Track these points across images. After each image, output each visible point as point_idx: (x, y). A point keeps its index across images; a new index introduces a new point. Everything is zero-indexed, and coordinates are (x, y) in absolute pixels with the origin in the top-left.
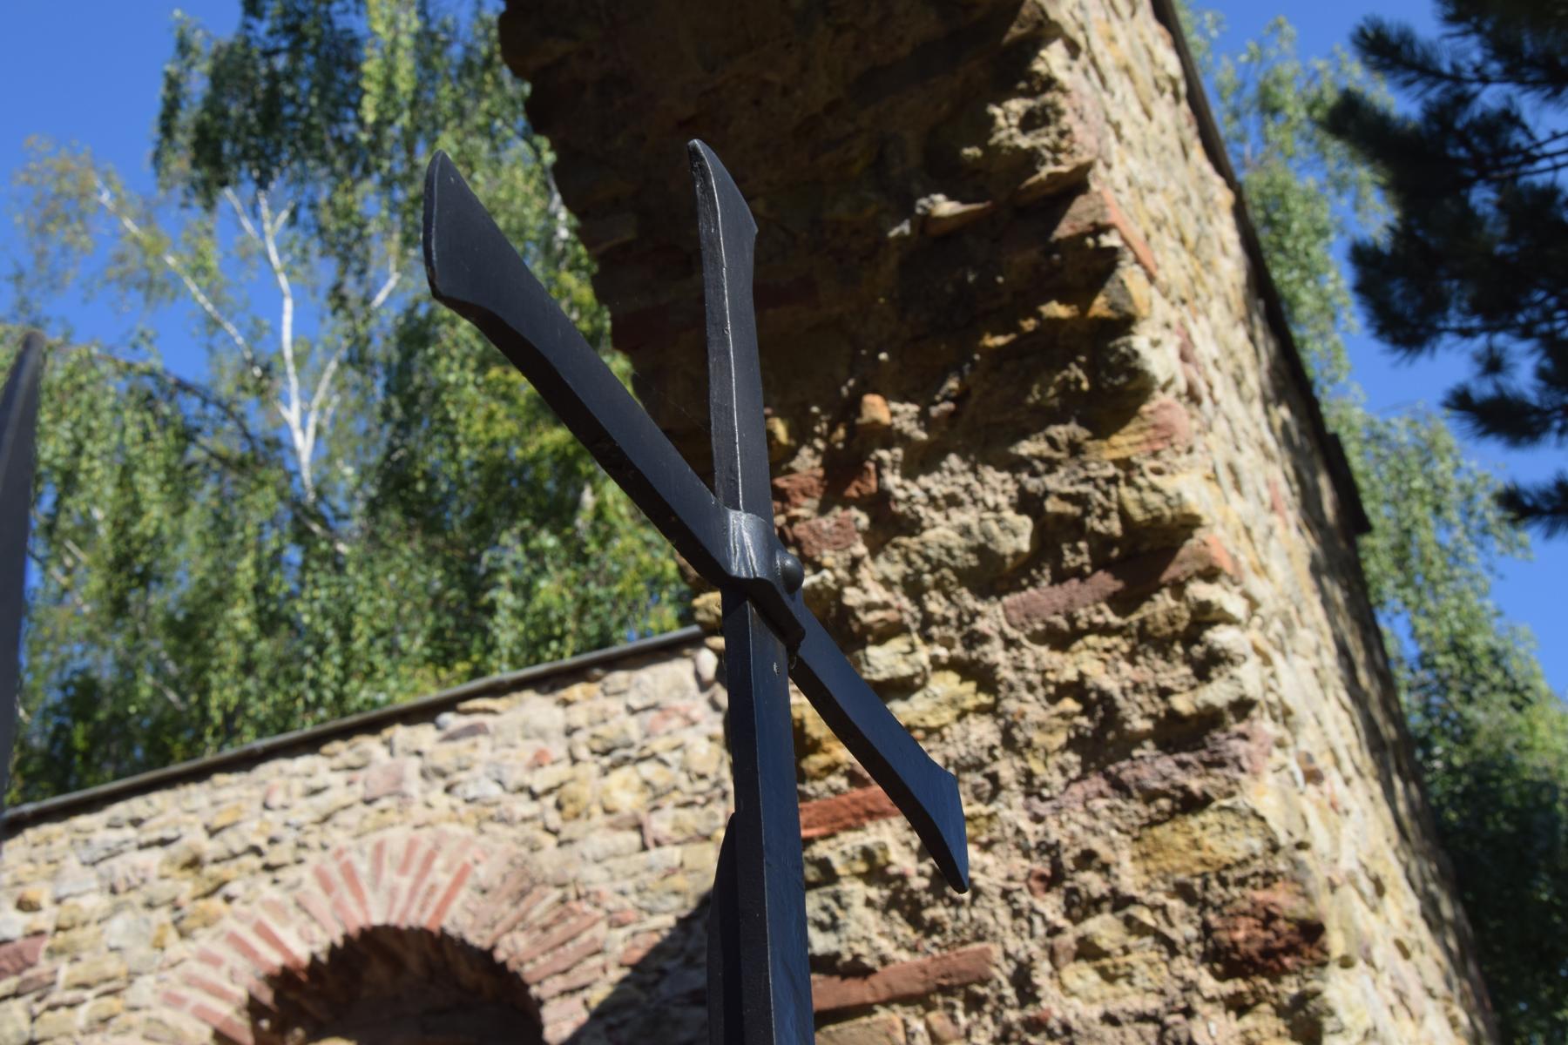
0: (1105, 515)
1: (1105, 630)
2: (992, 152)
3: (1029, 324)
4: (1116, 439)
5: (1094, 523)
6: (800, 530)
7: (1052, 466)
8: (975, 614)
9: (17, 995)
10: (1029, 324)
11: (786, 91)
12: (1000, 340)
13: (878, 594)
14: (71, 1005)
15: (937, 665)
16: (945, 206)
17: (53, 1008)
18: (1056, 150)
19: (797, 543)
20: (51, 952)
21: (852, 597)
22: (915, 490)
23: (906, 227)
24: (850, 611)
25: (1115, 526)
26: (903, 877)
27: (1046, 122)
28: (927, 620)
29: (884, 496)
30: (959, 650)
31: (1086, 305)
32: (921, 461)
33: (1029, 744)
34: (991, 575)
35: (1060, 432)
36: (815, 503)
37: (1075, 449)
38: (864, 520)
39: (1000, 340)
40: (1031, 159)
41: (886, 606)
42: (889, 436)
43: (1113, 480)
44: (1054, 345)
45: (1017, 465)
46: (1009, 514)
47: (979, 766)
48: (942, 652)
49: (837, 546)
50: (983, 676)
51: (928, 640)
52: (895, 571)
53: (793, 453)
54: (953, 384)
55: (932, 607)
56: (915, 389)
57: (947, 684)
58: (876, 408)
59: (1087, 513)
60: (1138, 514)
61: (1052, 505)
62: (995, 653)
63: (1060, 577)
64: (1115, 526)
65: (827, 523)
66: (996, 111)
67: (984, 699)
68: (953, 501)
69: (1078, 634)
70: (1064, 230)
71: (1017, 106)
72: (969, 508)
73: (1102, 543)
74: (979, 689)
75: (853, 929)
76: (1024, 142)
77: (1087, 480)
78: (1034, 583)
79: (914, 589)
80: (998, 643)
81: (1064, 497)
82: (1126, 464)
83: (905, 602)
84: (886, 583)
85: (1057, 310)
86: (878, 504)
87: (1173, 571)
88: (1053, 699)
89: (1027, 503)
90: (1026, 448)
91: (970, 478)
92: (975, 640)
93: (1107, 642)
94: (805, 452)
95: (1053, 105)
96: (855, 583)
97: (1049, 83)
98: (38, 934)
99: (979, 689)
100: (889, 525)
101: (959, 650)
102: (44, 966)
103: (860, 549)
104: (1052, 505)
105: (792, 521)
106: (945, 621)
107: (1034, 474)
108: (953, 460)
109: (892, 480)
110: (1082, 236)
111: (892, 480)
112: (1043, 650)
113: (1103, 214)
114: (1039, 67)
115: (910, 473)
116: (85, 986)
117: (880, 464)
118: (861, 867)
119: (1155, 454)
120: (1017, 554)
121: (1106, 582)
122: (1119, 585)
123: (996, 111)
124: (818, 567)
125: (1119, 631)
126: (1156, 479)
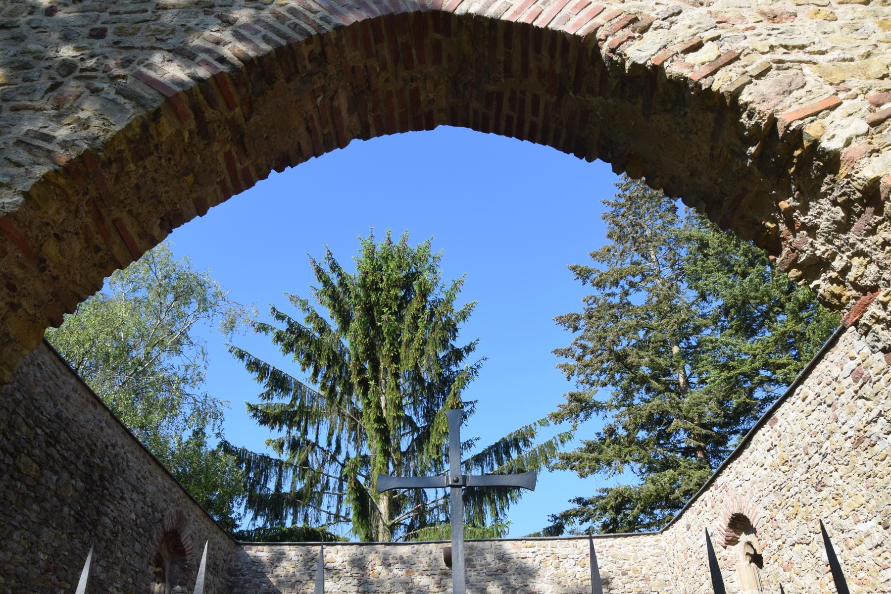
0: (855, 194)
1: (880, 222)
2: (749, 130)
3: (795, 161)
4: (840, 171)
5: (853, 197)
6: (794, 245)
7: (832, 190)
8: (848, 239)
9: (865, 383)
10: (795, 161)
11: (701, 154)
12: (793, 169)
13: (823, 248)
14: (878, 381)
15: (850, 258)
16: (752, 149)
17: (874, 383)
18: (761, 118)
19: (796, 248)
20: (866, 368)
21: (818, 253)
22: (810, 217)
23: (750, 161)
24: (820, 257)
25: (858, 195)
26: (884, 319)
27: (753, 114)
28: (839, 248)
29: (804, 224)
30: (852, 251)
31: (802, 146)
32: (805, 210)
33: (886, 265)
34: (843, 227)
35: (827, 180)
36: (791, 236)
37: (834, 181)
38: (805, 232)
39: (793, 169)
40: (757, 124)
41: (827, 250)
42: (792, 209)
43: (848, 183)
44: (804, 163)
45: (825, 195)
46: (833, 209)
47: (879, 278)
48: (848, 253)
49: (805, 243)
50: (860, 254)
51: (843, 252)
52: (822, 240)
53: (778, 227)
54: (793, 187)
55: (837, 244)
56: (789, 194)
57: (856, 261)
58: (784, 205)
59: (849, 196)
60: (861, 188)
61: (839, 200)
62: (860, 246)
63: (859, 216)
64: (858, 195)
65: (798, 239)
66: (741, 120)
67: (867, 259)
68: (820, 214)
69: (875, 228)
70: (781, 134)
71: (744, 115)
72: (825, 212)
73: (859, 200)
74: (864, 258)
75: (883, 338)
76: (753, 122)
77: (842, 187)
78: (854, 221)
79: (830, 242)
80: (859, 243)
81: (840, 196)
82: (848, 176)
83: (831, 246)
84: (823, 244)
85: (797, 153)
86: (804, 226)
87: (883, 196)
88: (883, 249)
89: (834, 203)
90: (823, 189)
91: (818, 205)
92: (853, 245)
93: (884, 225)
94: (780, 225)
95: (751, 109)
96: (816, 249)
97: (746, 104)
98: (859, 364)
99: (864, 258)
100: (812, 230)
101: (852, 251)
102: (866, 373)
103: (810, 240)
104: (839, 200)
105: (790, 243)
106: (843, 245)
107: (830, 195)
108: (811, 203)
109: (802, 219)
110: (785, 132)
111: (802, 219)
112: (870, 237)
113: (626, 232)
114: (741, 102)
115: (805, 214)
116: (879, 374)
117: (796, 217)
118: (874, 321)
119: (853, 168)
120: (843, 218)
121: (870, 210)
122: (873, 208)
123: (741, 120)
124: (802, 251)
125: (884, 220)
126: (857, 175)
